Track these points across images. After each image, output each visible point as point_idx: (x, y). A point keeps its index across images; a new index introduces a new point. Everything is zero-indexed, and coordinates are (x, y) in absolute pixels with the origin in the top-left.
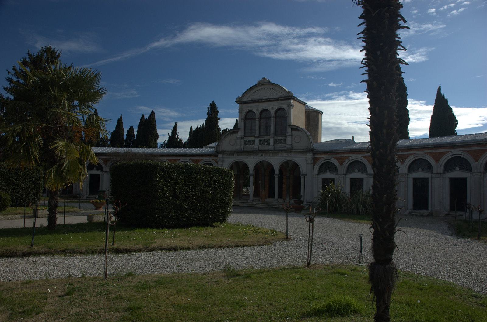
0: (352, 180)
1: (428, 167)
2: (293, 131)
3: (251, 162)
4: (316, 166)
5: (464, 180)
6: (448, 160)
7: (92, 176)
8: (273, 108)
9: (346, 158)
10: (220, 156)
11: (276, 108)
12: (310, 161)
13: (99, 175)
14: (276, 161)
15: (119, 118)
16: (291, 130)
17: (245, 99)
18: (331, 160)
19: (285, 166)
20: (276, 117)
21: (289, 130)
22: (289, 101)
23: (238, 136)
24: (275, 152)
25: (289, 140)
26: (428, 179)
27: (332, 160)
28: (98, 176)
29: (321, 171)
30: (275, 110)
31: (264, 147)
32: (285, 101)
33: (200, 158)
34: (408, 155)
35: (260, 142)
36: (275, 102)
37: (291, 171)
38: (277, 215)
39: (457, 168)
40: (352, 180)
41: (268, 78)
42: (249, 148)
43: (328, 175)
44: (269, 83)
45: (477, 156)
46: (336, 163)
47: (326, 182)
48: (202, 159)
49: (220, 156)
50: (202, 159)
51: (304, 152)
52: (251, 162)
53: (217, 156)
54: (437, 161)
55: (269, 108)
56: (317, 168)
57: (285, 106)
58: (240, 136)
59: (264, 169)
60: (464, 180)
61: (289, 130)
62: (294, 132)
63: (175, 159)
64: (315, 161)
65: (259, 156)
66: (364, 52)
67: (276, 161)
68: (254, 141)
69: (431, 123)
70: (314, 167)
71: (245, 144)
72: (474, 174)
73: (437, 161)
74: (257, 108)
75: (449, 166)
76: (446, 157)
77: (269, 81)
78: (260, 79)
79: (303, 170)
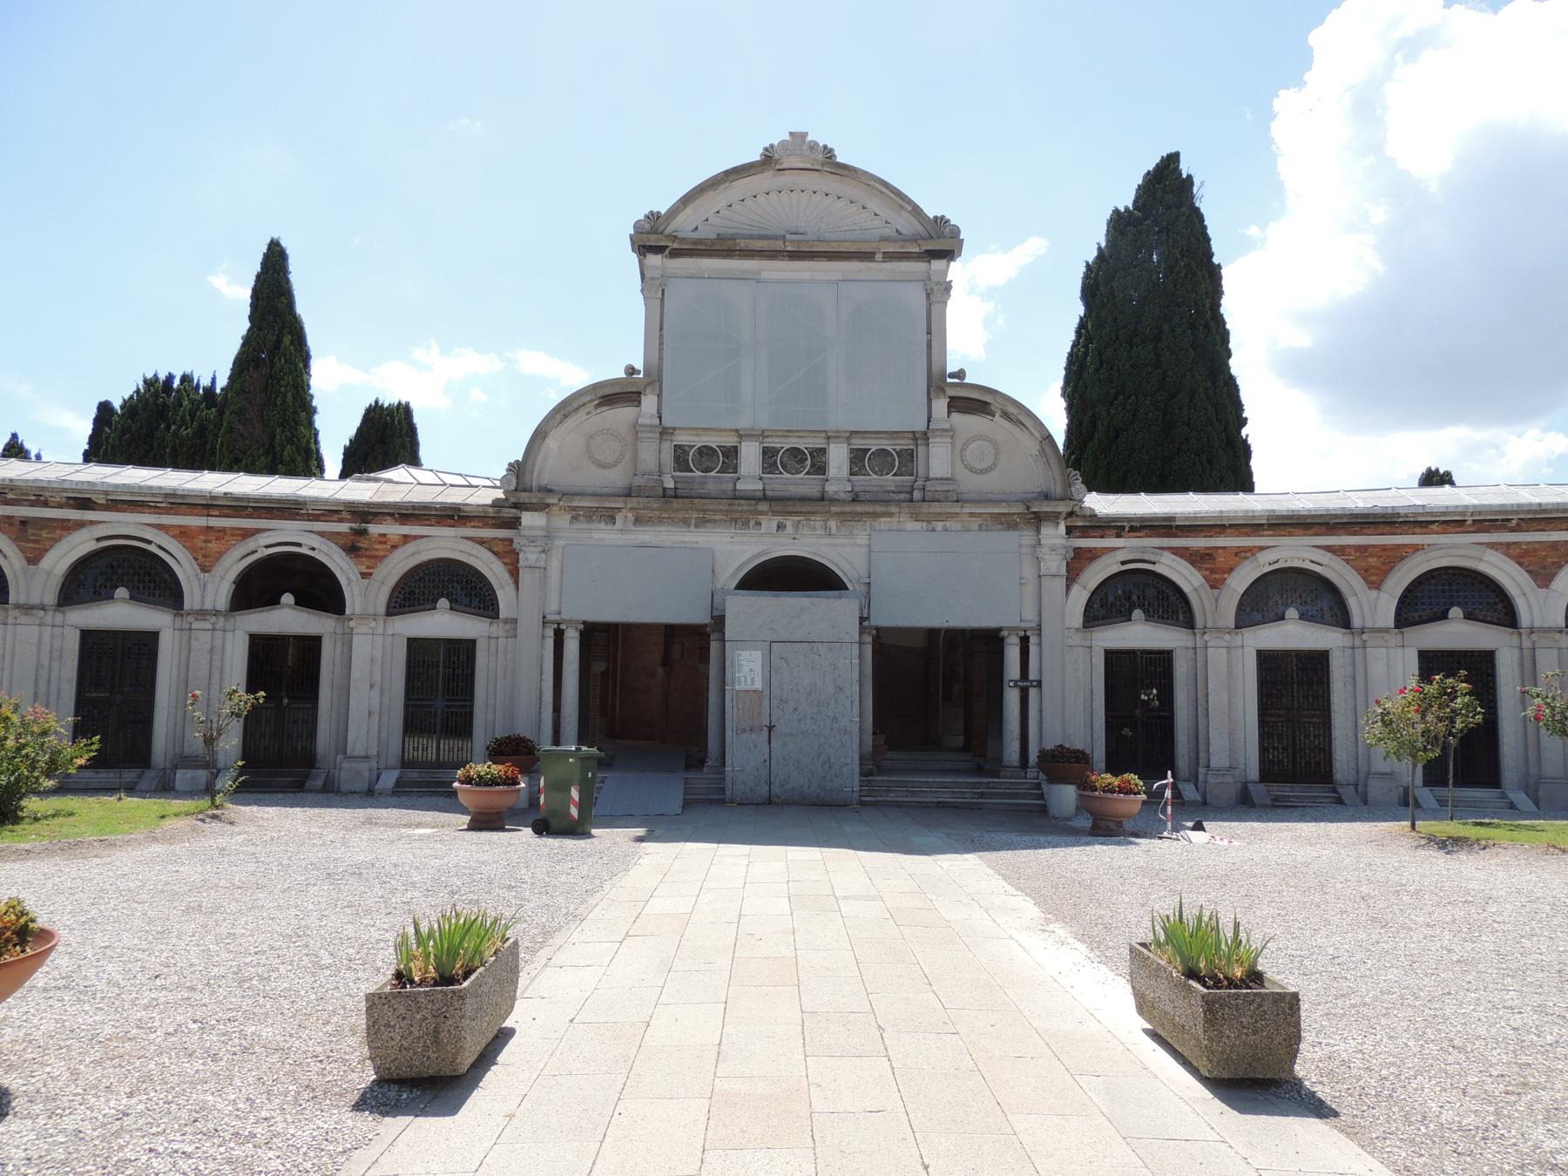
0: (1267, 660)
1: (1327, 603)
2: (955, 415)
4: (1076, 588)
5: (146, 643)
7: (264, 651)
9: (1242, 554)
12: (1055, 564)
13: (472, 643)
15: (663, 208)
16: (949, 406)
17: (684, 225)
18: (254, 552)
22: (937, 264)
26: (473, 642)
27: (1163, 560)
28: (1316, 663)
29: (1108, 605)
32: (919, 267)
33: (393, 530)
34: (1242, 554)
39: (122, 592)
40: (1267, 660)
42: (800, 483)
44: (827, 162)
45: (1543, 570)
48: (406, 539)
50: (405, 536)
53: (514, 523)
56: (1080, 596)
60: (146, 643)
63: (223, 530)
64: (1078, 562)
65: (763, 529)
69: (360, 430)
72: (190, 619)
73: (1215, 584)
75: (256, 588)
76: (1180, 568)
77: (828, 153)
78: (778, 136)
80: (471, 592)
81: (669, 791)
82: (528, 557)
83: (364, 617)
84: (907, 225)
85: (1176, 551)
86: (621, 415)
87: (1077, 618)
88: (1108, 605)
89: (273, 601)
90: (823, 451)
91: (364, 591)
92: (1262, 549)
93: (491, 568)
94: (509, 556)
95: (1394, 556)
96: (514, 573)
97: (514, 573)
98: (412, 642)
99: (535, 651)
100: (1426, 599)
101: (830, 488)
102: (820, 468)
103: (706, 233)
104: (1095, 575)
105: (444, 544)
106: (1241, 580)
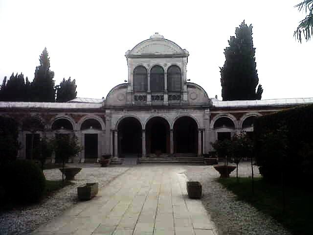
3: (144, 118)
4: (212, 121)
6: (168, 123)
8: (166, 65)
10: (107, 111)
11: (169, 64)
12: (208, 117)
14: (171, 117)
19: (180, 122)
20: (169, 74)
21: (185, 87)
23: (128, 91)
24: (169, 108)
25: (185, 97)
29: (218, 124)
30: (167, 67)
31: (157, 103)
32: (181, 58)
33: (81, 114)
35: (153, 98)
36: (168, 59)
37: (187, 127)
38: (114, 167)
40: (87, 136)
41: (161, 34)
42: (142, 103)
43: (224, 130)
46: (233, 118)
47: (222, 136)
48: (83, 115)
49: (107, 111)
51: (202, 108)
52: (144, 118)
54: (238, 119)
55: (162, 64)
56: (213, 123)
57: (179, 64)
58: (130, 91)
59: (158, 124)
61: (185, 87)
62: (189, 89)
64: (212, 116)
66: (248, 26)
67: (171, 117)
68: (145, 97)
70: (210, 122)
71: (136, 99)
73: (238, 119)
74: (149, 64)
79: (201, 125)
80: (97, 125)
81: (135, 160)
82: (107, 118)
83: (76, 131)
84: (179, 51)
85: (231, 113)
86: (125, 90)
87: (212, 127)
88: (218, 124)
89: (59, 128)
90: (163, 96)
91: (77, 127)
92: (246, 113)
93: (100, 120)
94: (104, 118)
95: (242, 114)
96: (105, 121)
97: (105, 121)
98: (85, 134)
99: (109, 135)
100: (87, 124)
101: (165, 103)
102: (162, 99)
103: (139, 54)
104: (215, 119)
105: (90, 116)
106: (243, 119)
